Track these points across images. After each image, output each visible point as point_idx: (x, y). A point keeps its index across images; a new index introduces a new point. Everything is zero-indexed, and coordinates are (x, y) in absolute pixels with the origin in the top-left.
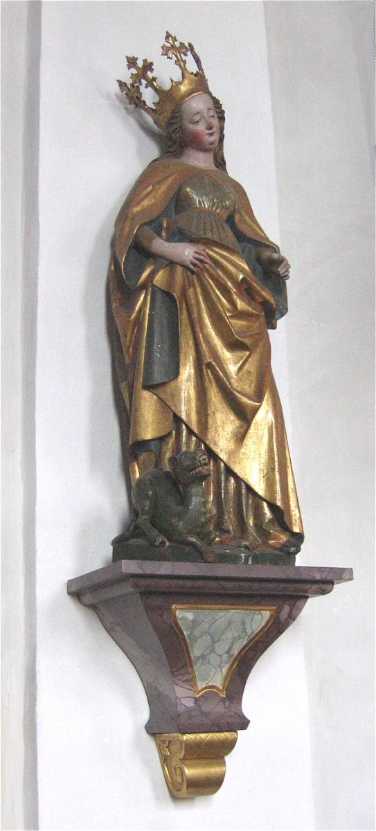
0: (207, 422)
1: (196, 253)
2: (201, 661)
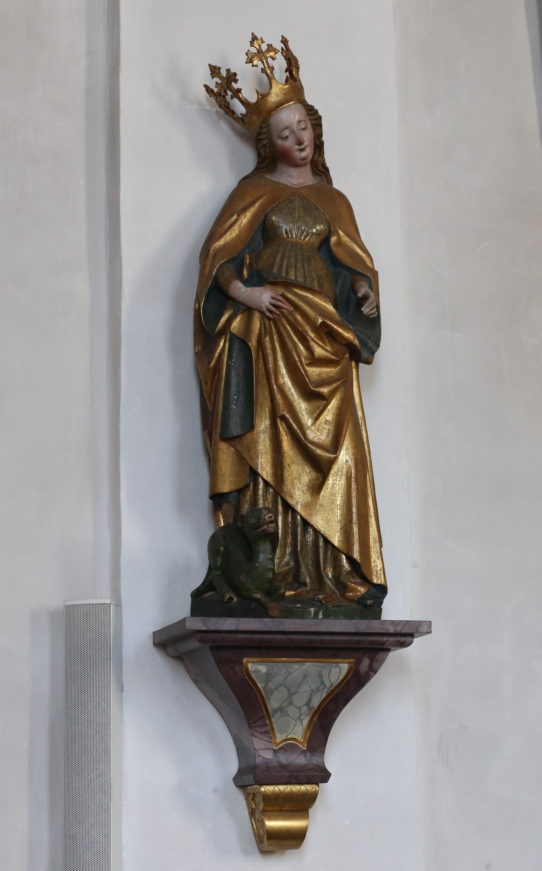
0: (282, 475)
1: (273, 298)
2: (278, 714)
